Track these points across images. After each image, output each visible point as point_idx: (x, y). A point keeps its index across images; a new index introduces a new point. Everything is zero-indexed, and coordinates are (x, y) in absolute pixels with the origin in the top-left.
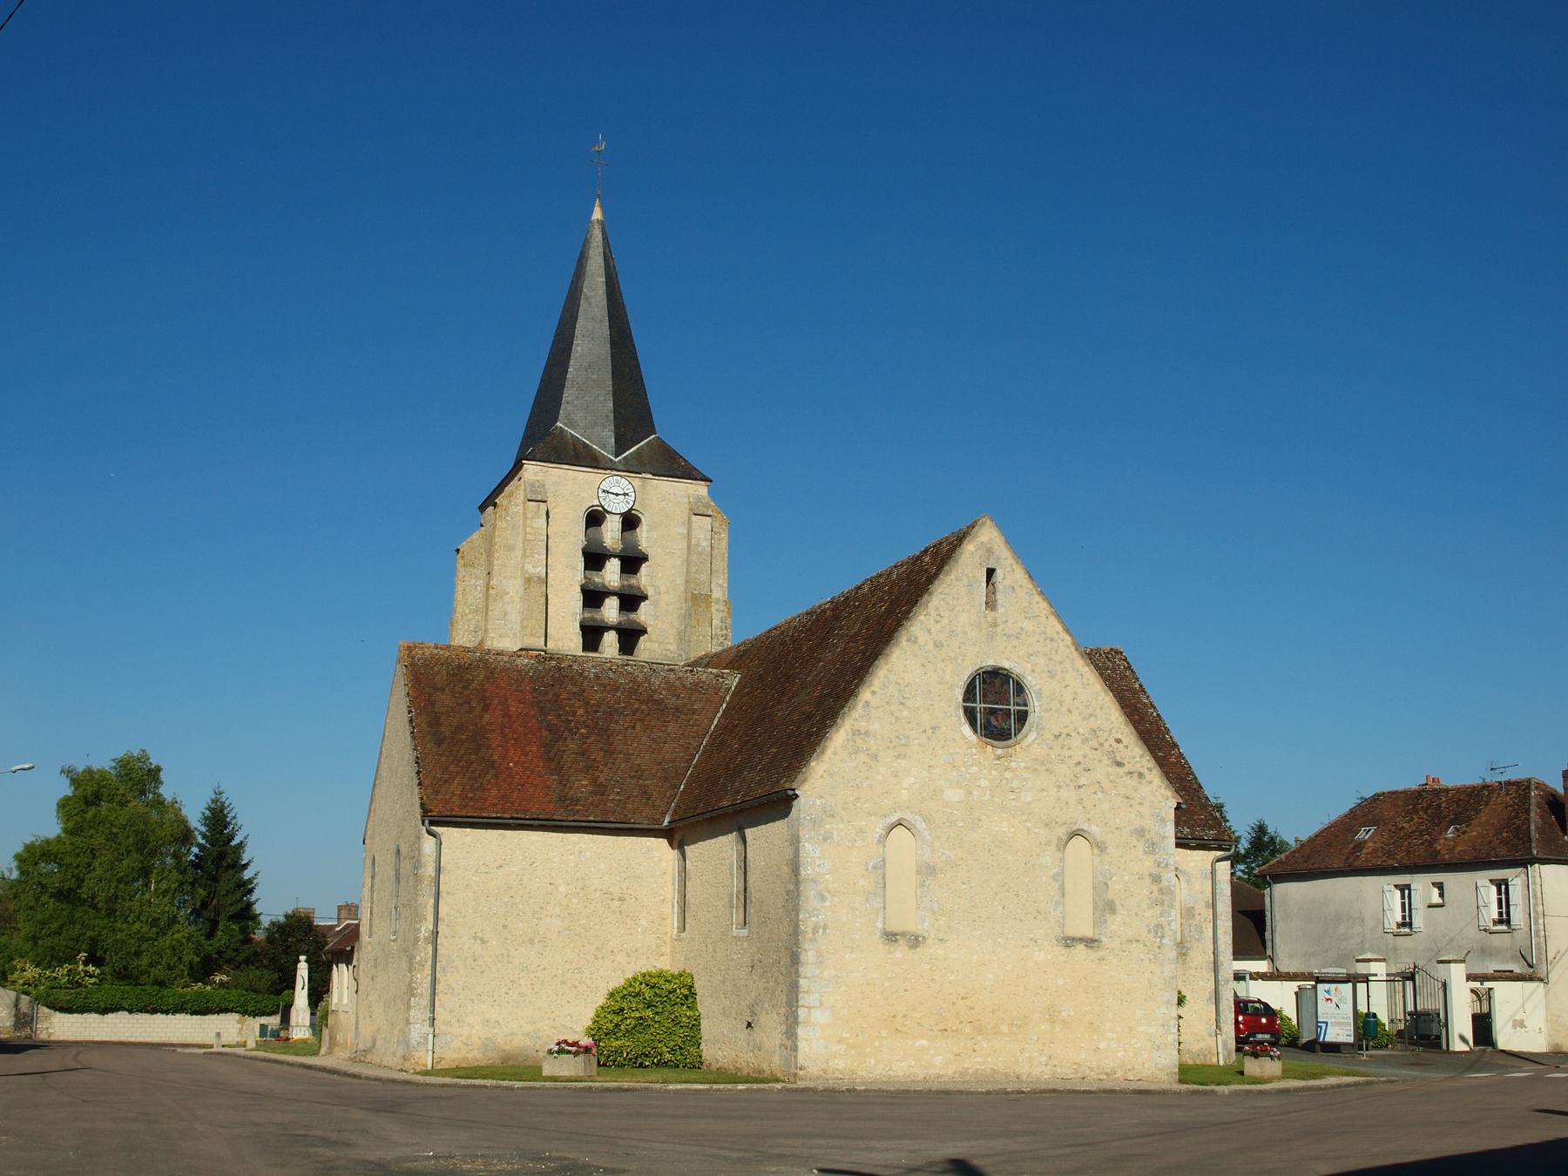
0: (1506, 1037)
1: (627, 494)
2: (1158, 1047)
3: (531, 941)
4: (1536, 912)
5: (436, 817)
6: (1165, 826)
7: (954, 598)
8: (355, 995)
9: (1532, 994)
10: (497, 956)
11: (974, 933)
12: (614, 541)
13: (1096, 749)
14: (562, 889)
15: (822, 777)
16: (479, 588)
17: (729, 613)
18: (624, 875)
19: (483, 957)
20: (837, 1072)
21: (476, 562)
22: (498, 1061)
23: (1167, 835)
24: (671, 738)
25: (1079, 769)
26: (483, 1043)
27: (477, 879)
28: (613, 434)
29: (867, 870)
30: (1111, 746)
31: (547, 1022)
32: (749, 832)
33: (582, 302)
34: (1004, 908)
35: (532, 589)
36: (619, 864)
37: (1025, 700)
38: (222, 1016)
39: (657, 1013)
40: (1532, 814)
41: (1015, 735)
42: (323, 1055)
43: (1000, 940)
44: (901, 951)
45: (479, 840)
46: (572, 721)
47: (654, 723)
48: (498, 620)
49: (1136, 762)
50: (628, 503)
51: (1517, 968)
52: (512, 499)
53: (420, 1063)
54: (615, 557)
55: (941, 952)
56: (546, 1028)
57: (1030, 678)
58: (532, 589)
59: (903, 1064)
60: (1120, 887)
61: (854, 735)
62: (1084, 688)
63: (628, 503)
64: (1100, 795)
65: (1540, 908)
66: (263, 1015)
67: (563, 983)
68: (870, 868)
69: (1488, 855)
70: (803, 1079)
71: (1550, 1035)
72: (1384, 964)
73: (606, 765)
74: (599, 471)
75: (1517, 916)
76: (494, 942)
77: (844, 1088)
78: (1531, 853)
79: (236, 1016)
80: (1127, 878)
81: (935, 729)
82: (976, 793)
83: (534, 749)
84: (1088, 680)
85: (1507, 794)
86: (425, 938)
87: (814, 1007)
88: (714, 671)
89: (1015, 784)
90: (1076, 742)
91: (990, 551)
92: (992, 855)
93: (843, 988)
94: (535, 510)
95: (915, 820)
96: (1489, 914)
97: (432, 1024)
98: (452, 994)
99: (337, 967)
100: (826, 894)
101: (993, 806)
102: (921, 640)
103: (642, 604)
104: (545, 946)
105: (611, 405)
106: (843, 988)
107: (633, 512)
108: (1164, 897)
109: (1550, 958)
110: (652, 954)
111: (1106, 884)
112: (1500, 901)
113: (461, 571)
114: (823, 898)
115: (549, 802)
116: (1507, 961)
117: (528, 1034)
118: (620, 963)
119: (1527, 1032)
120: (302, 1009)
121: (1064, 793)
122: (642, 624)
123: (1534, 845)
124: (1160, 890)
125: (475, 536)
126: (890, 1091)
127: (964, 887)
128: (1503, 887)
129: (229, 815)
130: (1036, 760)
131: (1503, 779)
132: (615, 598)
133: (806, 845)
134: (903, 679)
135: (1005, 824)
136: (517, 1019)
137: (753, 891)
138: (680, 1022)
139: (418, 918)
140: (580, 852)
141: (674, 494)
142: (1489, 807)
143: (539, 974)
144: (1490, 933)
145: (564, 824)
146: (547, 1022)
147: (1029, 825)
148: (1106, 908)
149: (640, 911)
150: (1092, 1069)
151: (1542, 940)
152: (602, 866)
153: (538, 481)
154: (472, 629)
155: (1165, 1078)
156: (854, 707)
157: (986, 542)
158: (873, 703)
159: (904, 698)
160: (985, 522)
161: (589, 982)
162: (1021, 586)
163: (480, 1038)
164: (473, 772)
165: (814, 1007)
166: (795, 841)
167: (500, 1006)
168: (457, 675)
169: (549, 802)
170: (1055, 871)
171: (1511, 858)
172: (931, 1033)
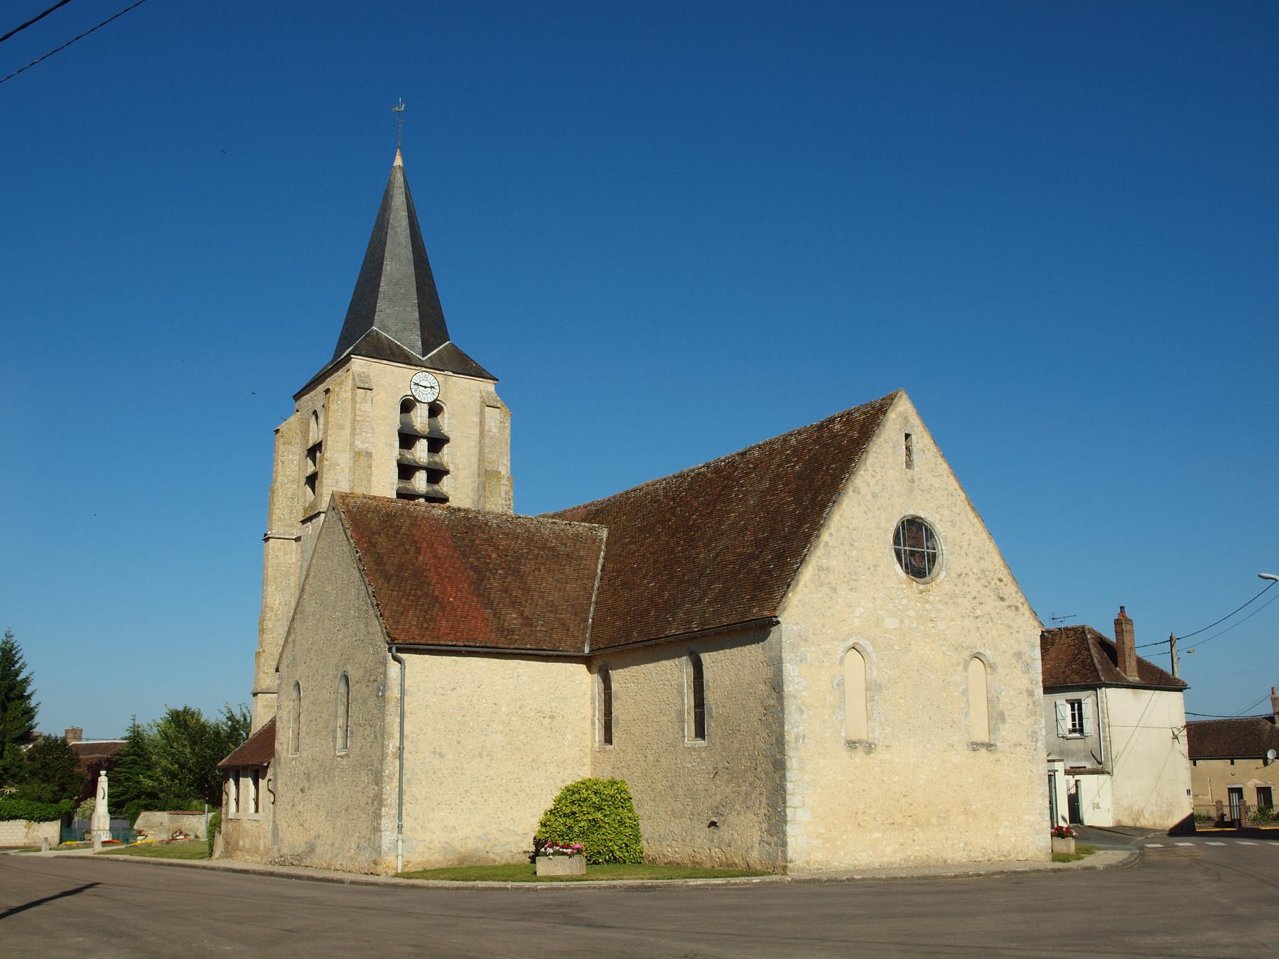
0: (1090, 817)
1: (433, 387)
2: (1038, 831)
3: (480, 755)
4: (1104, 723)
5: (402, 646)
6: (1035, 650)
7: (884, 457)
8: (271, 806)
9: (1105, 782)
10: (453, 769)
11: (911, 741)
12: (423, 425)
13: (986, 587)
14: (504, 709)
15: (797, 606)
16: (295, 462)
17: (511, 487)
18: (553, 696)
20: (817, 863)
22: (456, 863)
23: (1036, 657)
24: (570, 579)
25: (975, 602)
26: (443, 847)
27: (435, 700)
29: (833, 687)
30: (995, 584)
31: (494, 826)
32: (706, 658)
33: (389, 231)
34: (930, 718)
35: (361, 461)
36: (549, 687)
37: (934, 544)
38: (12, 822)
39: (605, 816)
40: (1092, 651)
41: (929, 573)
42: (217, 859)
43: (928, 746)
44: (859, 757)
45: (435, 665)
46: (490, 563)
47: (553, 566)
49: (1013, 598)
50: (434, 394)
51: (1089, 765)
52: (342, 386)
53: (391, 866)
54: (424, 438)
55: (888, 757)
56: (494, 832)
57: (938, 526)
58: (361, 461)
59: (864, 854)
60: (1007, 700)
61: (819, 570)
62: (976, 536)
63: (434, 394)
64: (991, 624)
65: (1106, 720)
66: (47, 821)
67: (507, 791)
68: (835, 685)
69: (1065, 682)
70: (792, 871)
71: (1115, 814)
72: (1062, 763)
73: (526, 601)
74: (411, 367)
75: (1089, 726)
76: (450, 756)
77: (844, 878)
78: (1101, 680)
79: (24, 822)
80: (1011, 693)
81: (875, 566)
82: (906, 621)
83: (466, 586)
84: (978, 529)
85: (1068, 637)
86: (393, 754)
87: (797, 807)
88: (587, 525)
89: (933, 614)
90: (971, 580)
91: (906, 420)
92: (920, 674)
93: (819, 790)
94: (363, 396)
95: (866, 645)
96: (1065, 724)
97: (400, 832)
98: (417, 804)
99: (237, 784)
100: (803, 708)
101: (919, 633)
102: (862, 492)
103: (445, 477)
104: (491, 759)
105: (417, 314)
106: (819, 790)
107: (437, 402)
108: (1036, 708)
109: (1113, 757)
110: (576, 764)
111: (998, 698)
112: (1073, 715)
113: (281, 448)
114: (802, 712)
115: (491, 632)
116: (1081, 760)
117: (479, 838)
118: (552, 773)
119: (1101, 812)
120: (103, 815)
121: (967, 623)
122: (445, 493)
123: (1100, 674)
124: (1034, 702)
126: (882, 878)
127: (902, 701)
128: (1076, 705)
129: (17, 656)
130: (947, 594)
131: (1063, 626)
132: (424, 471)
133: (788, 665)
134: (851, 523)
135: (928, 648)
136: (470, 824)
137: (713, 707)
138: (625, 823)
139: (382, 734)
140: (518, 676)
141: (469, 389)
142: (1055, 647)
143: (486, 784)
144: (1067, 739)
145: (508, 651)
146: (494, 826)
147: (944, 648)
148: (997, 718)
149: (566, 727)
150: (994, 852)
151: (1109, 743)
152: (535, 689)
153: (364, 372)
155: (1043, 857)
156: (818, 546)
157: (903, 413)
158: (831, 544)
159: (853, 540)
160: (902, 395)
161: (527, 790)
162: (929, 450)
163: (440, 842)
164: (423, 605)
165: (797, 807)
166: (776, 665)
167: (456, 813)
168: (387, 521)
169: (491, 632)
170: (963, 687)
171: (1085, 683)
172: (883, 826)
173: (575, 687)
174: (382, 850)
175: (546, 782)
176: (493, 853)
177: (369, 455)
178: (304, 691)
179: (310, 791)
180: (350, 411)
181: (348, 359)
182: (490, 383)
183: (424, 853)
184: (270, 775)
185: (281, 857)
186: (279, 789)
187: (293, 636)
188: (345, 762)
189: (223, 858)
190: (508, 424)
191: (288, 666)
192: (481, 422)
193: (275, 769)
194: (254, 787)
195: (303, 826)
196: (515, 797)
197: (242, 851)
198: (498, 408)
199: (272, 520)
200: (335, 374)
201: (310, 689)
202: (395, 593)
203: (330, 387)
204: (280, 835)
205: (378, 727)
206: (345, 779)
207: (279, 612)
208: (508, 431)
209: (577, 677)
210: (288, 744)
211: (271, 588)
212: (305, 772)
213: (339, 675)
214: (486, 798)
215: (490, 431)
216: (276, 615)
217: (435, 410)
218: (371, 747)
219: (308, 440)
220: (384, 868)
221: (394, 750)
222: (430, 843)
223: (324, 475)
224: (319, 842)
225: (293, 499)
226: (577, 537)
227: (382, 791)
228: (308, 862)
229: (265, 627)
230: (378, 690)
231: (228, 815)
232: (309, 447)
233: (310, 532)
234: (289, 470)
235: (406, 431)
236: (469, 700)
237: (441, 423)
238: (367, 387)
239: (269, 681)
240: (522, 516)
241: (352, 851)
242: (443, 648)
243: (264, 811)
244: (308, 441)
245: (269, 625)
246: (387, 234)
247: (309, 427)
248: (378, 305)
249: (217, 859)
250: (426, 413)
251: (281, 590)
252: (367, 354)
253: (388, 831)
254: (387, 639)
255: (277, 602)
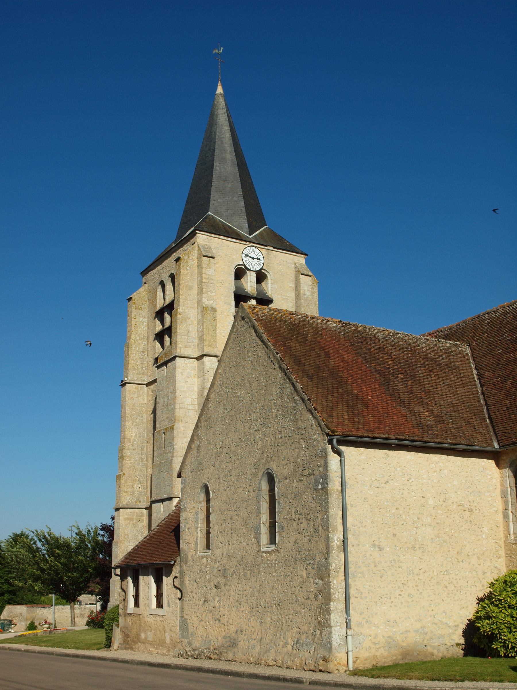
1: (259, 259)
8: (178, 601)
10: (391, 562)
12: (252, 288)
14: (431, 502)
16: (145, 323)
19: (381, 562)
21: (143, 307)
22: (400, 657)
27: (371, 493)
28: (246, 221)
31: (429, 619)
33: (216, 141)
42: (116, 650)
48: (184, 336)
50: (260, 265)
56: (429, 624)
63: (260, 265)
67: (438, 583)
74: (242, 242)
94: (208, 263)
98: (361, 598)
105: (243, 203)
107: (262, 271)
117: (417, 631)
118: (473, 565)
125: (142, 289)
145: (434, 445)
146: (429, 619)
152: (455, 482)
154: (141, 350)
163: (384, 637)
167: (396, 606)
173: (487, 481)
174: (333, 647)
175: (470, 575)
176: (431, 646)
177: (214, 310)
178: (213, 492)
179: (227, 587)
180: (196, 275)
181: (193, 234)
182: (301, 257)
183: (370, 647)
184: (175, 571)
185: (194, 650)
186: (187, 585)
187: (197, 443)
188: (273, 556)
189: (122, 649)
190: (316, 290)
191: (192, 471)
192: (296, 287)
193: (181, 567)
194: (155, 585)
195: (219, 620)
196: (445, 589)
197: (144, 643)
198: (310, 276)
199: (128, 369)
200: (181, 249)
201: (222, 489)
202: (320, 391)
203: (181, 256)
204: (191, 630)
205: (319, 521)
206: (274, 574)
207: (135, 442)
208: (316, 295)
209: (488, 472)
210: (197, 543)
211: (128, 424)
212: (220, 568)
213: (261, 474)
214: (421, 591)
215: (304, 294)
216: (133, 445)
217: (261, 277)
218: (310, 541)
219: (155, 306)
220: (335, 666)
221: (338, 543)
222: (375, 638)
223: (178, 326)
224: (241, 637)
225: (143, 352)
226: (447, 351)
227: (330, 585)
228: (230, 656)
229: (124, 455)
230: (317, 482)
231: (126, 610)
232: (157, 310)
233: (166, 374)
234: (140, 329)
235: (240, 293)
236: (401, 493)
237: (265, 288)
238: (210, 255)
239: (128, 498)
240: (399, 332)
241: (289, 647)
242: (378, 440)
243: (169, 605)
244: (155, 306)
245: (127, 453)
246: (215, 143)
247: (156, 295)
248: (211, 196)
249: (116, 650)
250: (254, 279)
251: (136, 425)
252: (208, 231)
253: (337, 626)
254: (327, 431)
255: (134, 434)
